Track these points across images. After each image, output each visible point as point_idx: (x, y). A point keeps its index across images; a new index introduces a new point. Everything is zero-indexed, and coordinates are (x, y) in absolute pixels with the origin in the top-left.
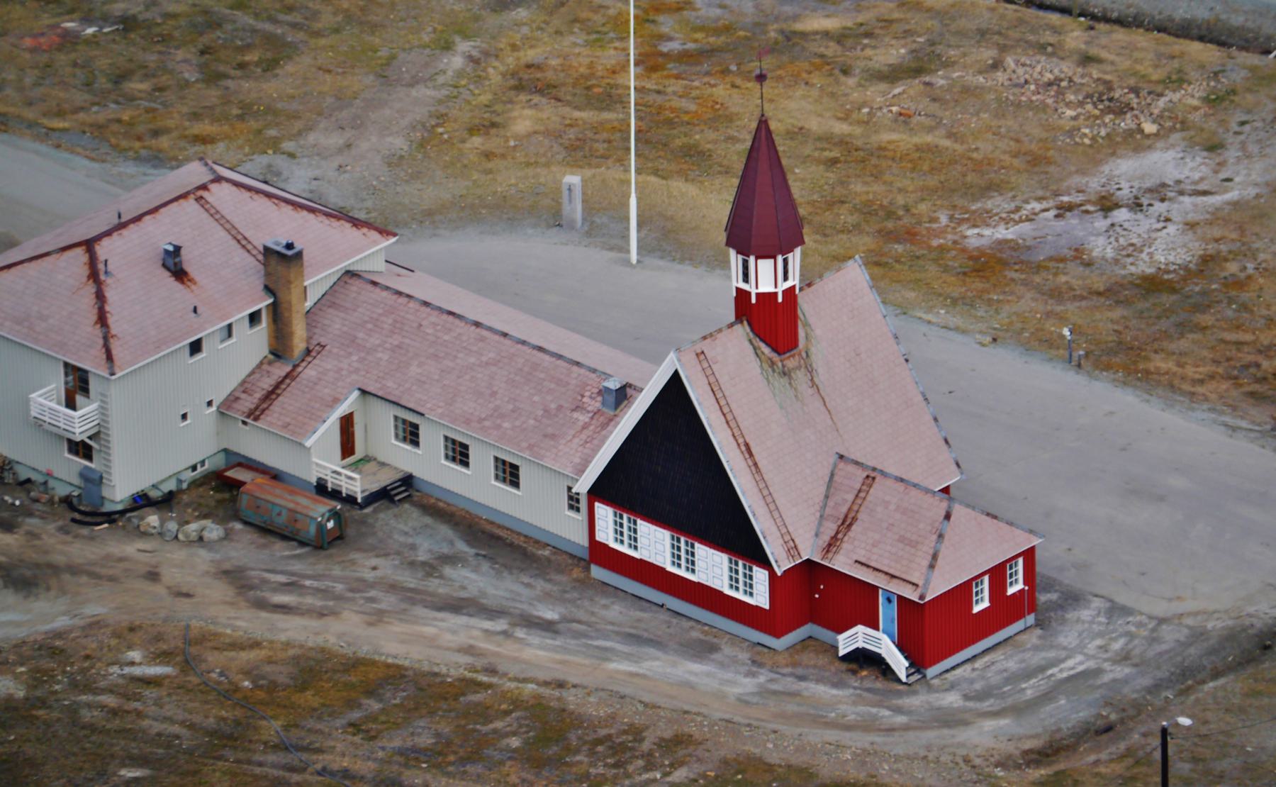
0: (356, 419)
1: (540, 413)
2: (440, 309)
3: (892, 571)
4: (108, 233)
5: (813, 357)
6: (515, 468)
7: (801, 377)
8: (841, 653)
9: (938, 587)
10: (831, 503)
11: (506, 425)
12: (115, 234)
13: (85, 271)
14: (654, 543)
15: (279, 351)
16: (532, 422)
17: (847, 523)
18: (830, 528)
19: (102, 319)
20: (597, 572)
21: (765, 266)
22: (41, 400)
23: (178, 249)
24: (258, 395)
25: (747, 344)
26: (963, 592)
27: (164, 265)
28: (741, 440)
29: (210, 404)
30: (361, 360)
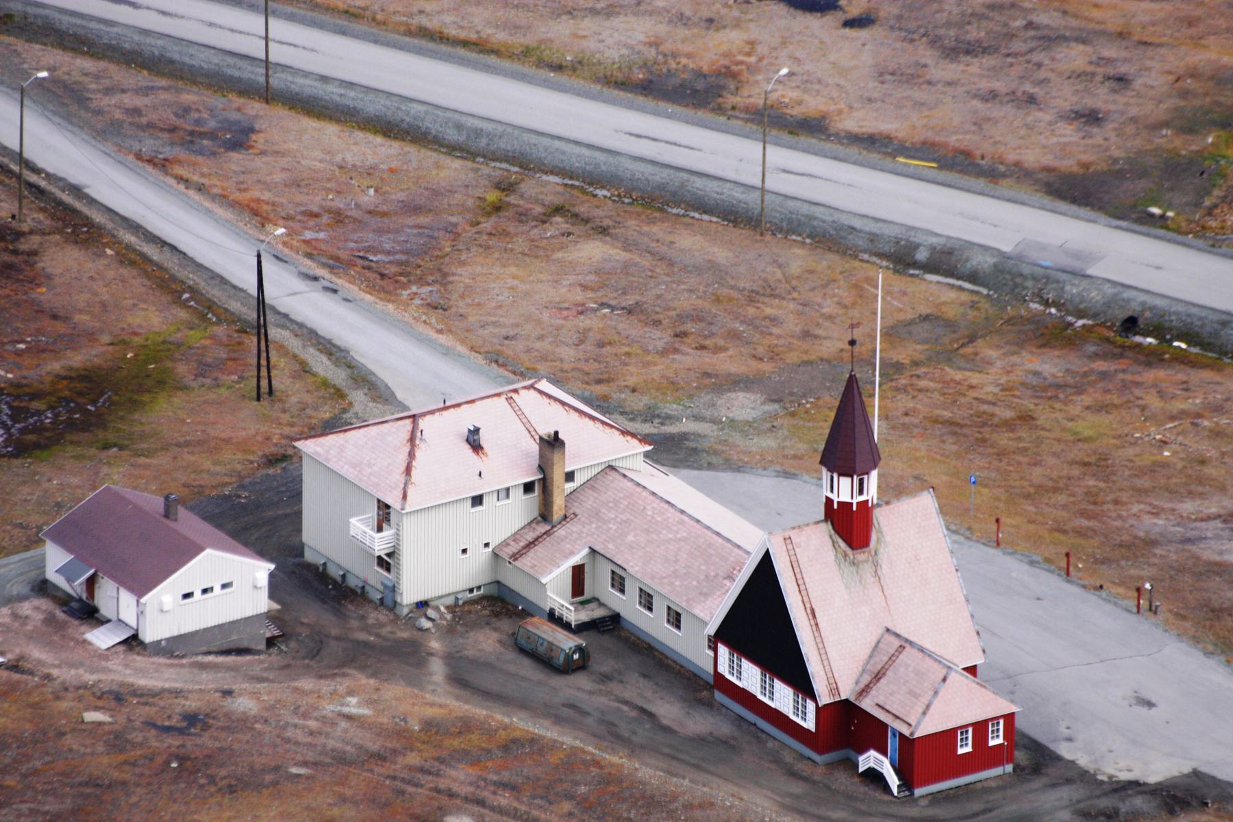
0: (587, 569)
1: (702, 577)
2: (661, 498)
3: (897, 714)
4: (432, 412)
5: (880, 556)
6: (678, 615)
7: (867, 569)
8: (861, 770)
9: (926, 728)
10: (872, 662)
11: (677, 583)
12: (437, 414)
13: (407, 436)
14: (750, 677)
15: (545, 515)
16: (695, 583)
17: (878, 677)
18: (866, 679)
19: (408, 470)
20: (719, 696)
21: (845, 482)
22: (358, 524)
23: (477, 430)
24: (522, 544)
25: (827, 538)
26: (948, 737)
27: (467, 440)
28: (808, 606)
29: (487, 545)
30: (598, 528)
